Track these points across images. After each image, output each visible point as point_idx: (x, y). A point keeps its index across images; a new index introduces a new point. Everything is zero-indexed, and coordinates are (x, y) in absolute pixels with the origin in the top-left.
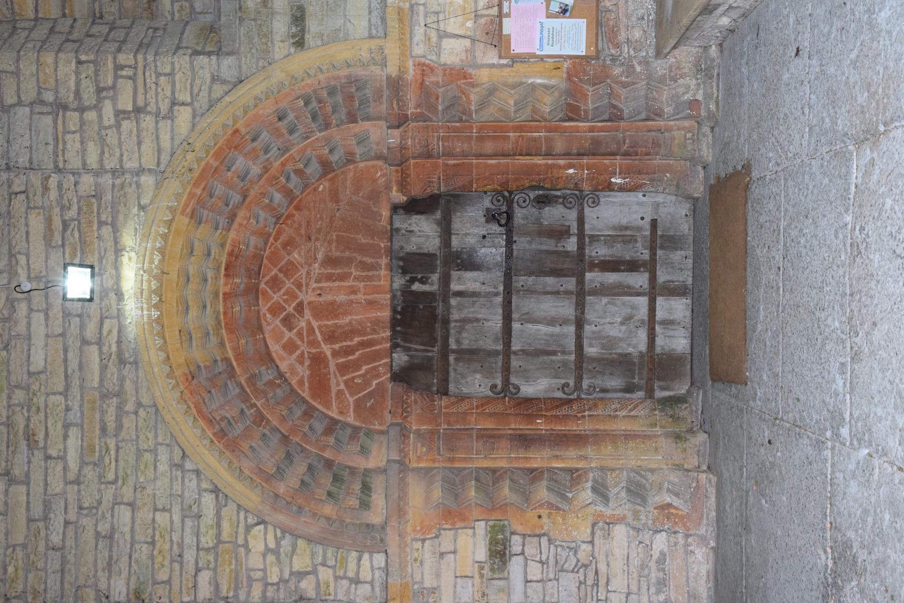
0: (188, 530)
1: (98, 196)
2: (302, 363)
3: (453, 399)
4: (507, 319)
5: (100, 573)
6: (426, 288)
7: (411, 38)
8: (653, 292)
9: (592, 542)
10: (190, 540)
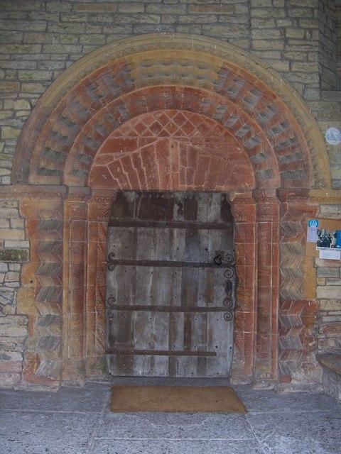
0: (29, 63)
1: (234, 15)
2: (130, 135)
3: (106, 229)
4: (155, 264)
5: (6, 13)
6: (175, 214)
7: (331, 205)
8: (171, 354)
9: (16, 314)
10: (24, 65)
